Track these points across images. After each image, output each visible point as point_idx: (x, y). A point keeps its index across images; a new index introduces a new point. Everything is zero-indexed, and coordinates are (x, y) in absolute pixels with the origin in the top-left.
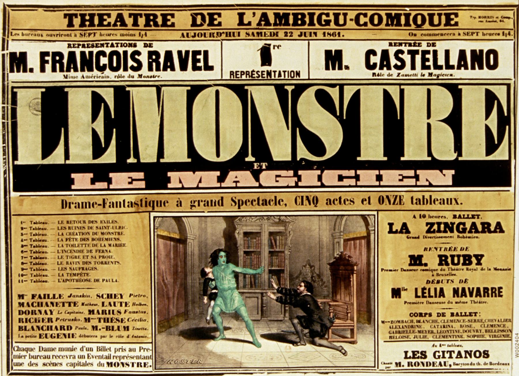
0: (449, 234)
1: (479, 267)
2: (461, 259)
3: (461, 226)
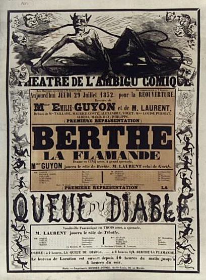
0: (164, 111)
1: (135, 112)
2: (91, 106)
3: (78, 106)
